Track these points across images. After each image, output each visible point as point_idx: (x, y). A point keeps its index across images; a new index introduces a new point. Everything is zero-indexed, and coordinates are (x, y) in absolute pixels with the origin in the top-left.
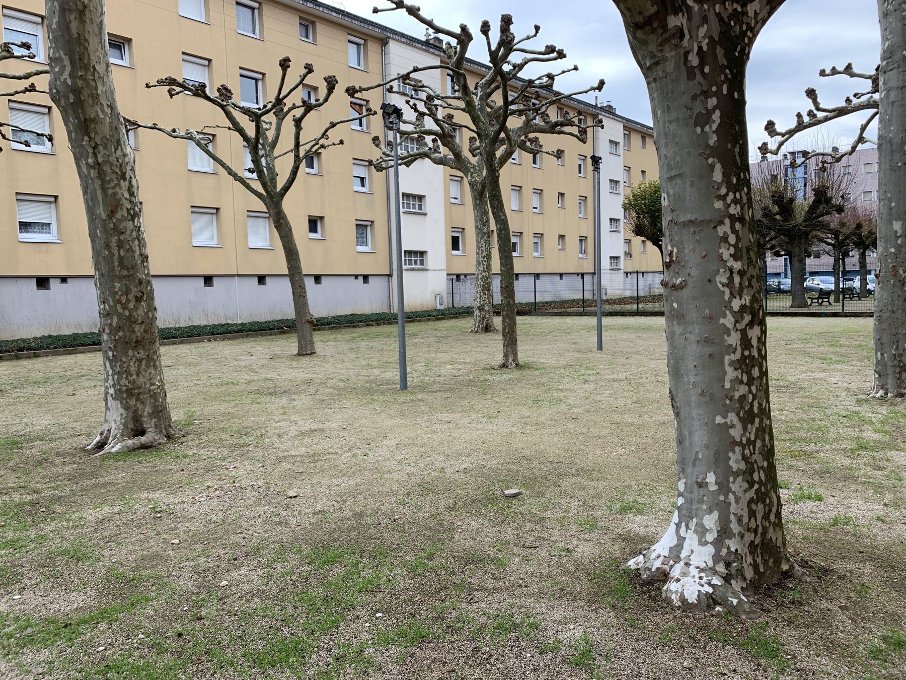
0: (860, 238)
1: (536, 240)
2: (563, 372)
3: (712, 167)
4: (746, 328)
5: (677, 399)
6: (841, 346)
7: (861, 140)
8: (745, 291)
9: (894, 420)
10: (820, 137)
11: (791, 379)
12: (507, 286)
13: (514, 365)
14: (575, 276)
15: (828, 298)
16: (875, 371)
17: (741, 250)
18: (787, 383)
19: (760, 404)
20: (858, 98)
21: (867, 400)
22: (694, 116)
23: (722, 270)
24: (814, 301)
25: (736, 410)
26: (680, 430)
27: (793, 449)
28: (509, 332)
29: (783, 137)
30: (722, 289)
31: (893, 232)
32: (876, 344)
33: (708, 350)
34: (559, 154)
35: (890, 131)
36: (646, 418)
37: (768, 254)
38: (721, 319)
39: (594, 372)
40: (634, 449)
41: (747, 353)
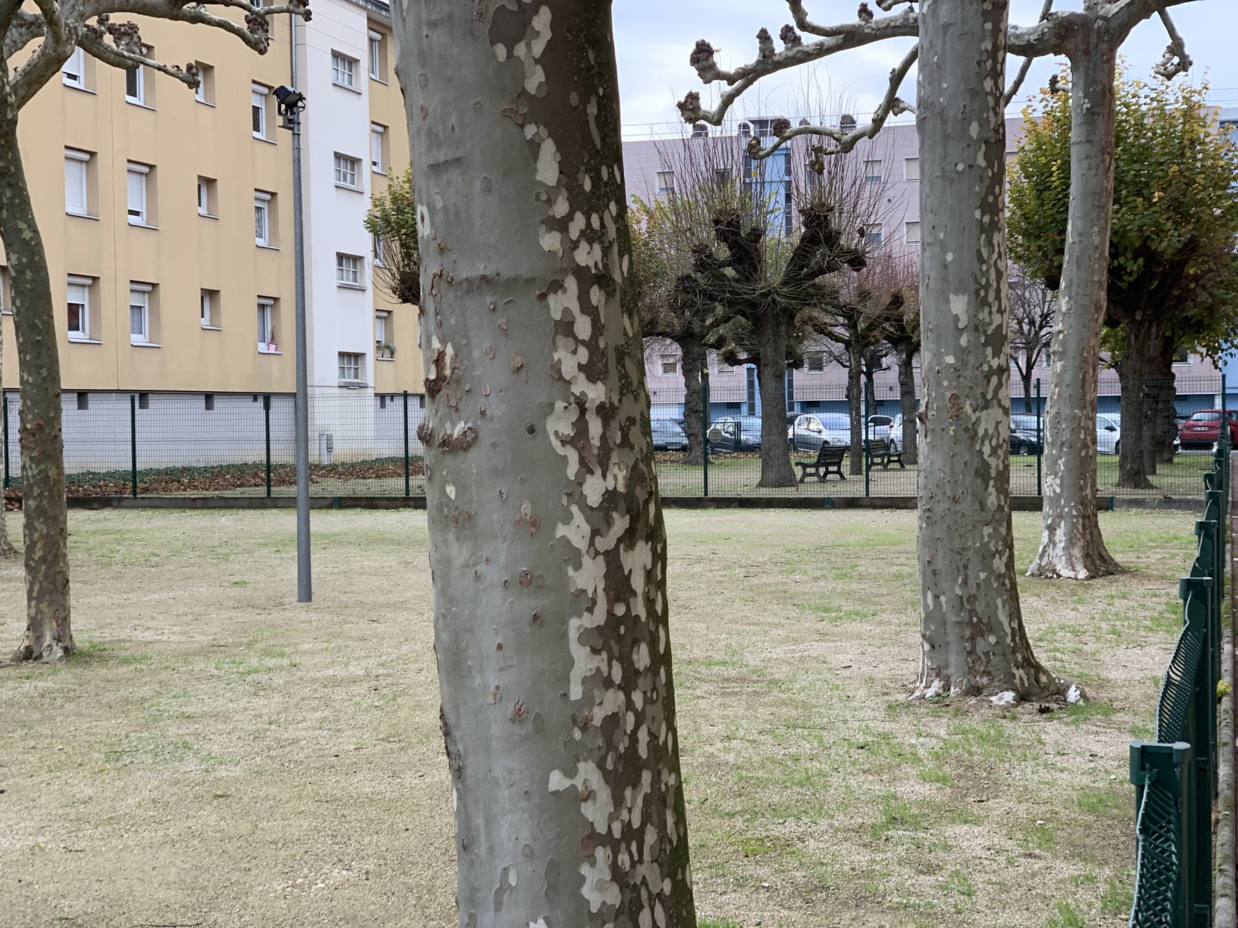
0: (901, 328)
1: (137, 300)
2: (199, 665)
3: (534, 148)
4: (617, 546)
5: (456, 733)
6: (861, 577)
7: (892, 104)
8: (615, 458)
9: (960, 750)
10: (813, 91)
11: (753, 661)
12: (40, 428)
13: (60, 653)
14: (249, 402)
15: (838, 464)
16: (924, 636)
17: (603, 354)
18: (744, 670)
19: (653, 736)
20: (886, 9)
21: (908, 706)
22: (490, 16)
23: (560, 405)
24: (809, 470)
25: (596, 754)
26: (464, 815)
27: (749, 835)
28: (43, 559)
29: (731, 83)
30: (560, 450)
31: (951, 319)
32: (924, 574)
33: (529, 604)
34: (195, 75)
35: (941, 92)
36: (409, 779)
37: (713, 357)
38: (560, 525)
39: (286, 662)
40: (371, 867)
41: (620, 610)
